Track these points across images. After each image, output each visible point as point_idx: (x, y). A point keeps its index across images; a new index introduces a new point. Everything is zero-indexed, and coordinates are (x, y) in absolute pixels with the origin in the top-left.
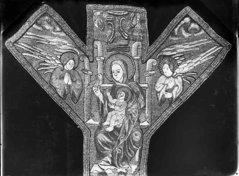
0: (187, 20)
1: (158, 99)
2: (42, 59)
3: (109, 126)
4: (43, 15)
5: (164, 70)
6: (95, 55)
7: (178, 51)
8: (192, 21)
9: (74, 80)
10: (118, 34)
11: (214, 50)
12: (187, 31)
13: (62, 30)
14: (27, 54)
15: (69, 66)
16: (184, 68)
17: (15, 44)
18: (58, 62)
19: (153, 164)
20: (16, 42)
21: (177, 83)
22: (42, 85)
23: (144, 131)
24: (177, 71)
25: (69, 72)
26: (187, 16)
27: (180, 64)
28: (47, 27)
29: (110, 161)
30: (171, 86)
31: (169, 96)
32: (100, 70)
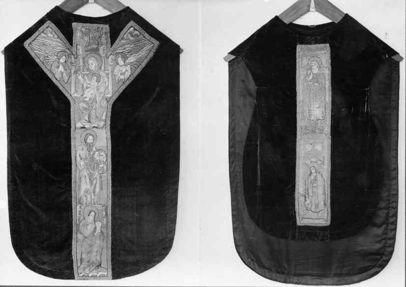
0: (132, 29)
1: (116, 80)
2: (46, 55)
3: (86, 97)
4: (47, 28)
5: (119, 62)
6: (78, 54)
7: (127, 49)
8: (135, 29)
9: (66, 68)
10: (91, 41)
11: (149, 47)
12: (132, 36)
13: (59, 37)
14: (38, 52)
15: (62, 60)
16: (132, 59)
17: (30, 45)
18: (56, 57)
19: (88, 1)
20: (30, 43)
21: (127, 69)
22: (43, 63)
23: (108, 100)
24: (127, 61)
25: (62, 64)
26: (132, 27)
27: (129, 57)
28: (50, 35)
29: (87, 120)
30: (124, 71)
31: (122, 77)
32: (81, 64)
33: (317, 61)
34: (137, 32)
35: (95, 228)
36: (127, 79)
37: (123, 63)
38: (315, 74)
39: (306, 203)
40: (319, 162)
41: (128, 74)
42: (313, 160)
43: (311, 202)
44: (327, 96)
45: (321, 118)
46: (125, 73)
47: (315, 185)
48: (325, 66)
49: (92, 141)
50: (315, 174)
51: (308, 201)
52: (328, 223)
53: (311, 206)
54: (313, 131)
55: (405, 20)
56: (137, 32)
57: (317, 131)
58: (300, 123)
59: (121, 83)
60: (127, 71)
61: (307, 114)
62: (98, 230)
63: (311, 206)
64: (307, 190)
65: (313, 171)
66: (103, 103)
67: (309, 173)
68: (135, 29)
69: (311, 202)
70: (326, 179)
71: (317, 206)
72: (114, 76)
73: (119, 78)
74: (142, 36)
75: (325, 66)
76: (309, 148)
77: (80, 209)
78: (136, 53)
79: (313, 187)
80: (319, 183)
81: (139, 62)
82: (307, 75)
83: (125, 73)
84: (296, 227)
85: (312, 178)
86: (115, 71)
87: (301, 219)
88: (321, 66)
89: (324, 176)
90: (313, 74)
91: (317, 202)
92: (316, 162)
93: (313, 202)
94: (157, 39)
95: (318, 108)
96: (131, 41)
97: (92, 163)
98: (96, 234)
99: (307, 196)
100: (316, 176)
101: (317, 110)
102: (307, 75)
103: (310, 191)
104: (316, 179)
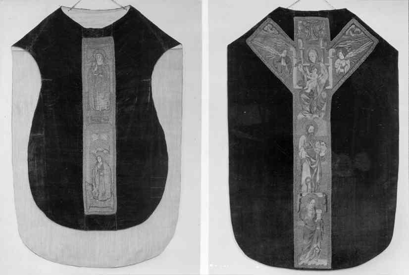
0: (353, 26)
3: (307, 89)
5: (340, 56)
7: (348, 44)
16: (351, 54)
24: (347, 56)
26: (353, 24)
29: (309, 110)
31: (342, 71)
33: (101, 54)
34: (358, 30)
35: (316, 215)
36: (346, 74)
37: (344, 57)
38: (100, 66)
39: (93, 192)
40: (105, 151)
41: (347, 69)
42: (100, 149)
43: (98, 191)
44: (112, 87)
45: (106, 108)
46: (345, 66)
47: (102, 174)
48: (109, 58)
49: (313, 131)
50: (101, 163)
51: (95, 190)
52: (115, 212)
53: (98, 195)
54: (98, 120)
55: (408, 27)
56: (358, 30)
57: (102, 121)
58: (86, 114)
59: (340, 77)
60: (347, 65)
61: (92, 105)
62: (319, 218)
63: (98, 195)
64: (93, 179)
65: (100, 160)
66: (324, 94)
67: (95, 162)
68: (356, 26)
69: (98, 191)
70: (112, 169)
71: (104, 194)
72: (334, 69)
73: (339, 70)
74: (362, 33)
75: (109, 58)
76: (95, 137)
77: (300, 197)
78: (356, 49)
79: (100, 175)
80: (105, 172)
81: (358, 56)
82: (92, 67)
83: (345, 66)
84: (84, 217)
85: (99, 167)
86: (336, 64)
87: (88, 208)
88: (106, 58)
89: (110, 165)
90: (98, 66)
91: (104, 190)
92: (102, 151)
93: (100, 191)
94: (378, 38)
95: (103, 99)
96: (352, 37)
97: (312, 155)
98: (316, 221)
99: (94, 184)
100: (102, 166)
101: (102, 100)
102: (92, 67)
103: (97, 180)
104: (102, 168)
